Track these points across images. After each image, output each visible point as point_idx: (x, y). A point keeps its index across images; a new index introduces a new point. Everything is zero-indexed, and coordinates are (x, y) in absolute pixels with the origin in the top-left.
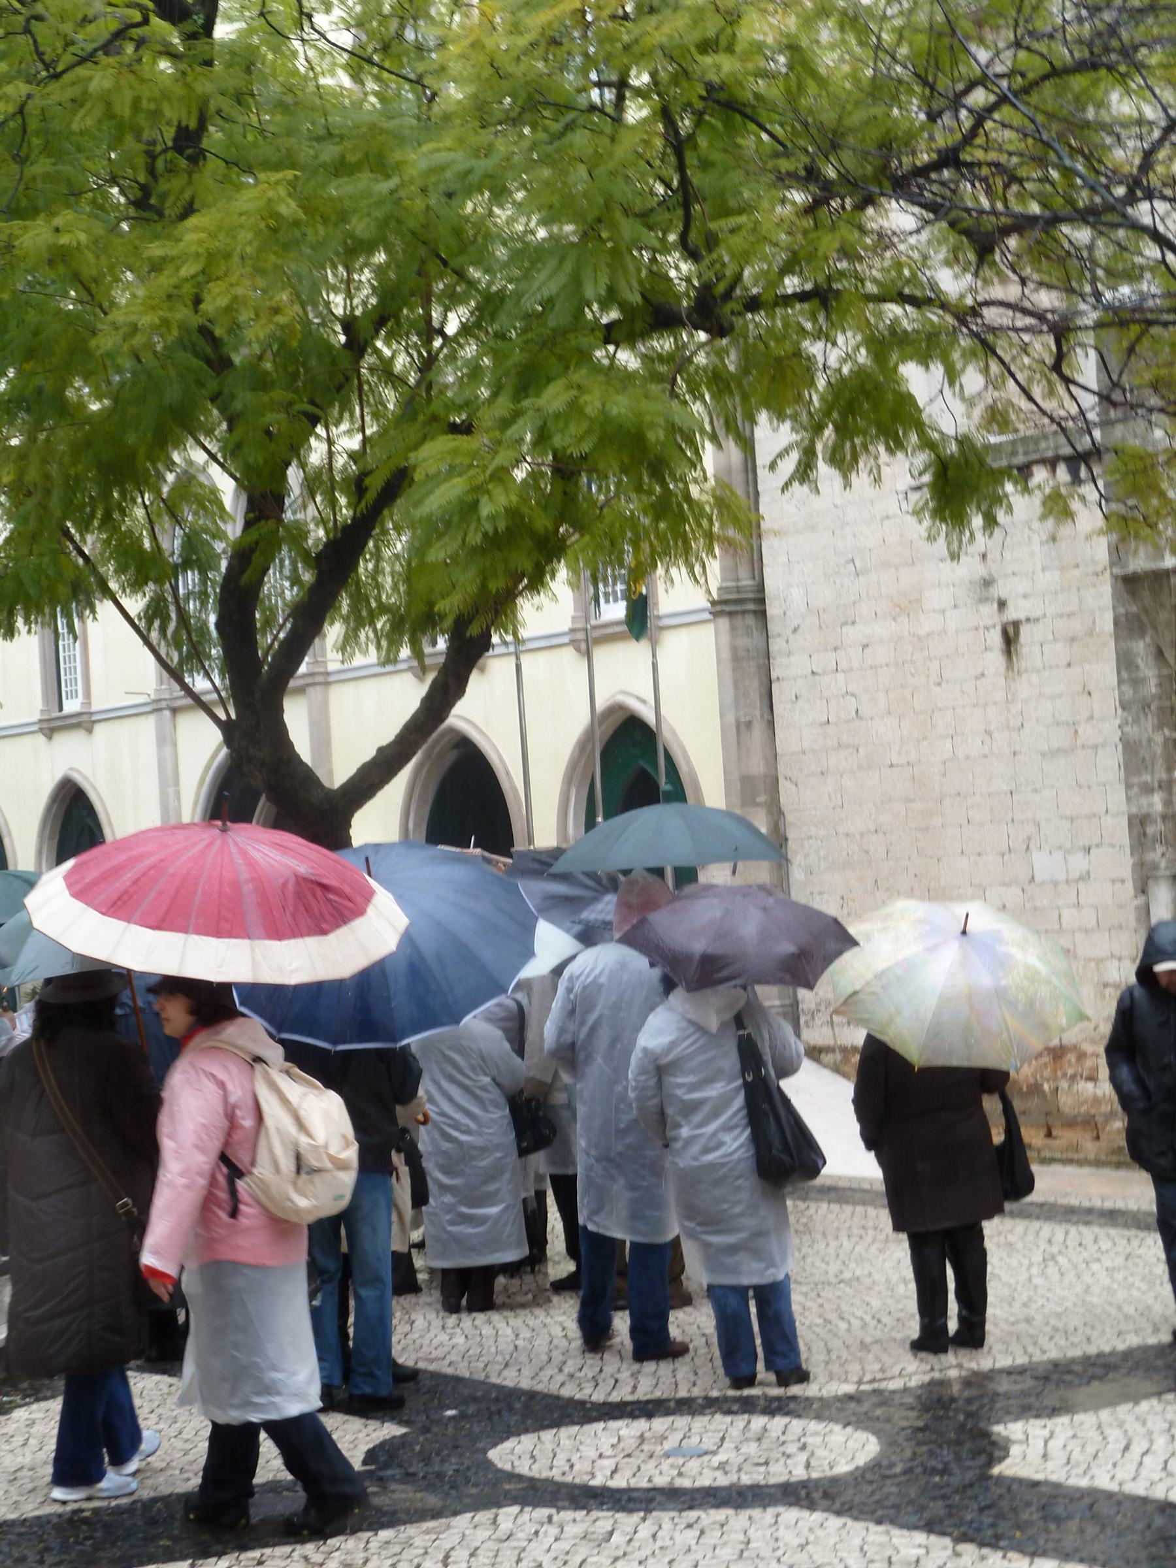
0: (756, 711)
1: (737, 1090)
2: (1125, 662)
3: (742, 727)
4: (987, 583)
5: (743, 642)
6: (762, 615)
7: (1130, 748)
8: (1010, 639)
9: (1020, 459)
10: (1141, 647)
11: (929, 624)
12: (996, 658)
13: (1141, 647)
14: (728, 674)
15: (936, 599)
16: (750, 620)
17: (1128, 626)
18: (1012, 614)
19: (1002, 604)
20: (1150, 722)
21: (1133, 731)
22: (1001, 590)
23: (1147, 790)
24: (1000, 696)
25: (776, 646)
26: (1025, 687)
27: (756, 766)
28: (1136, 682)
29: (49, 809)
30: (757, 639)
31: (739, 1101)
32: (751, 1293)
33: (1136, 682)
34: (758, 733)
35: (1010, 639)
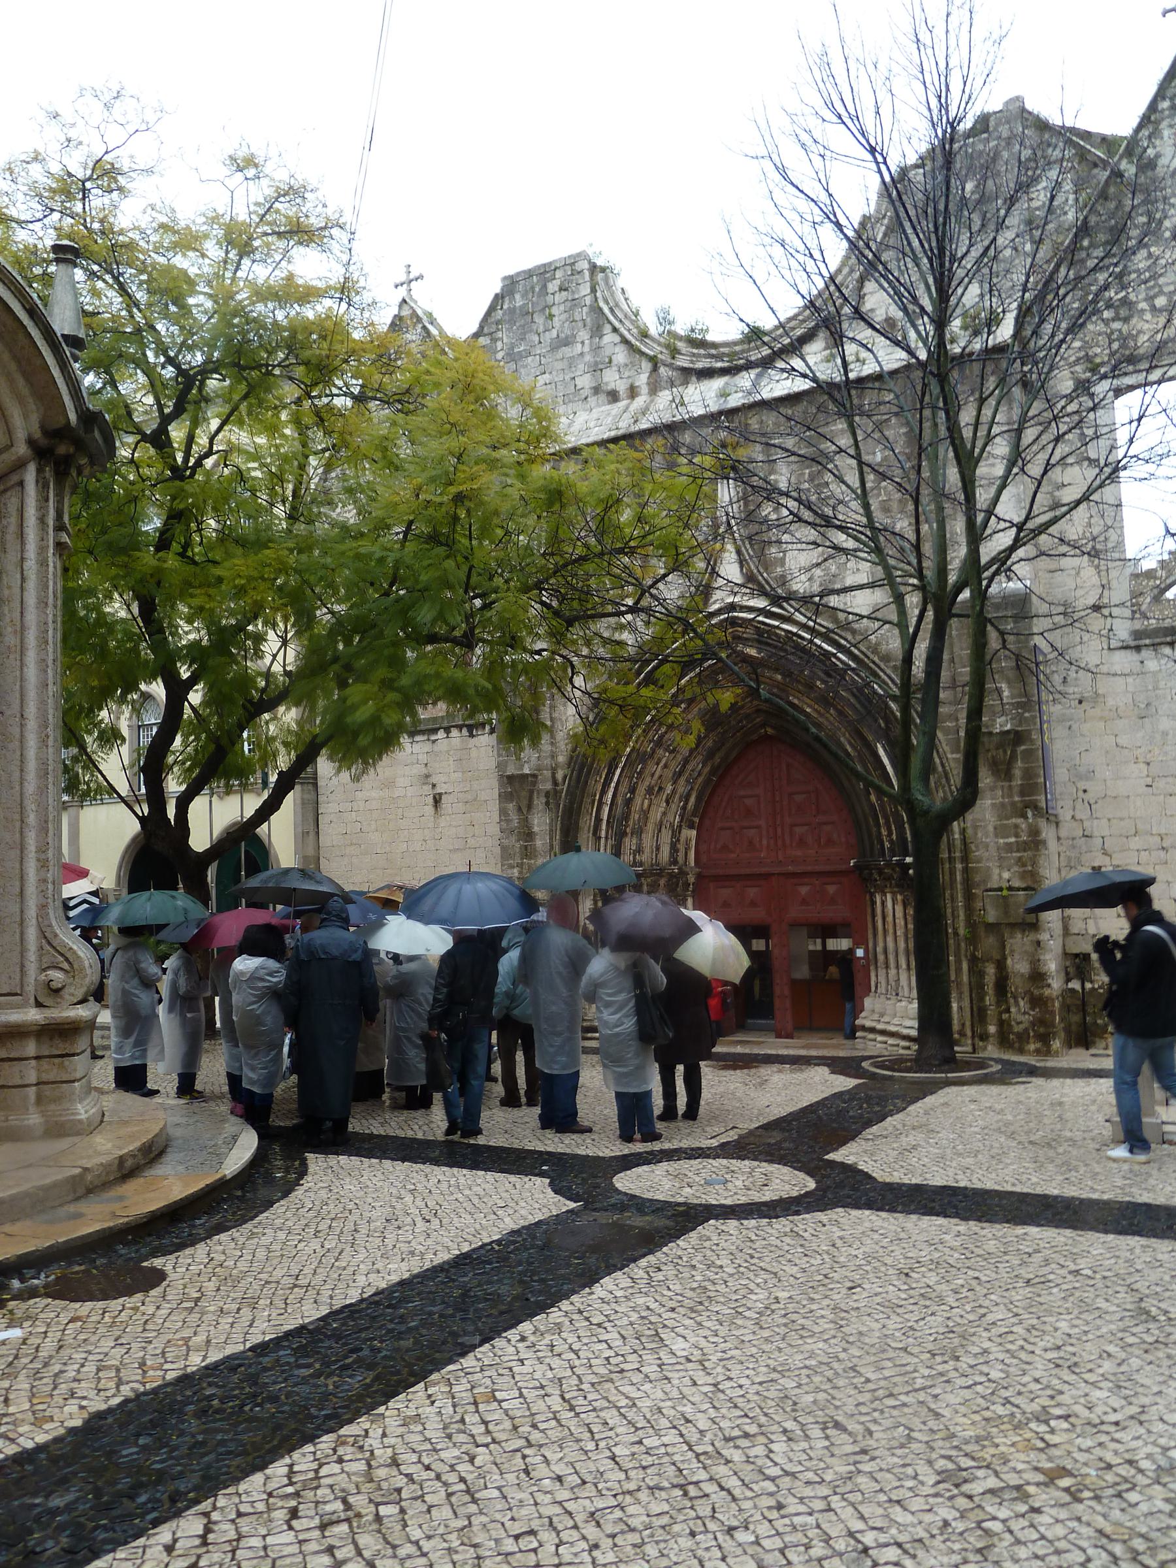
0: (312, 827)
1: (629, 1000)
2: (503, 812)
3: (305, 834)
4: (427, 776)
5: (306, 796)
6: (316, 785)
7: (504, 848)
8: (437, 800)
9: (445, 724)
10: (511, 806)
11: (398, 793)
12: (430, 809)
13: (511, 806)
14: (299, 810)
15: (401, 782)
16: (310, 787)
17: (505, 797)
18: (438, 790)
19: (434, 786)
20: (513, 838)
21: (506, 842)
22: (434, 779)
23: (512, 867)
24: (431, 825)
25: (321, 799)
26: (443, 822)
27: (310, 851)
28: (508, 821)
29: (123, 858)
30: (312, 796)
31: (632, 1004)
32: (524, 1100)
33: (508, 821)
34: (312, 835)
35: (437, 800)
